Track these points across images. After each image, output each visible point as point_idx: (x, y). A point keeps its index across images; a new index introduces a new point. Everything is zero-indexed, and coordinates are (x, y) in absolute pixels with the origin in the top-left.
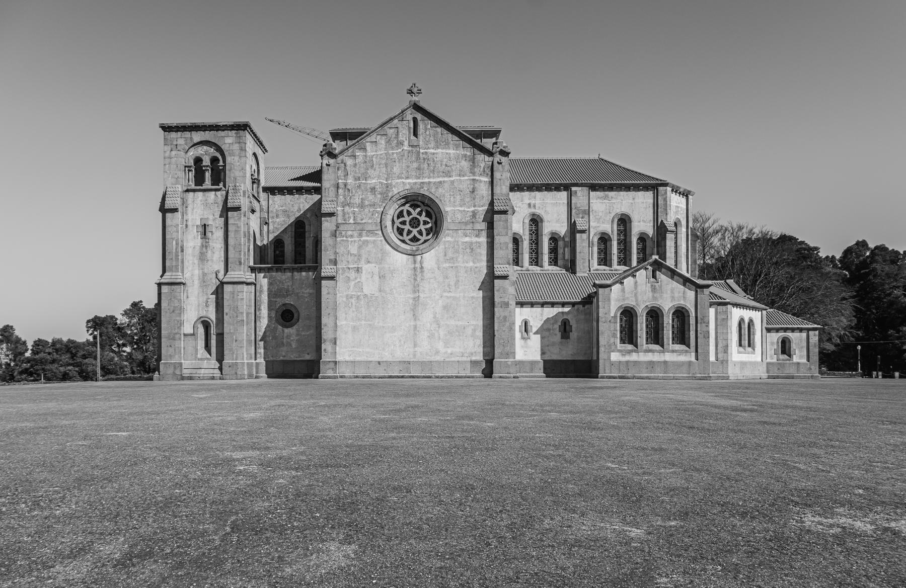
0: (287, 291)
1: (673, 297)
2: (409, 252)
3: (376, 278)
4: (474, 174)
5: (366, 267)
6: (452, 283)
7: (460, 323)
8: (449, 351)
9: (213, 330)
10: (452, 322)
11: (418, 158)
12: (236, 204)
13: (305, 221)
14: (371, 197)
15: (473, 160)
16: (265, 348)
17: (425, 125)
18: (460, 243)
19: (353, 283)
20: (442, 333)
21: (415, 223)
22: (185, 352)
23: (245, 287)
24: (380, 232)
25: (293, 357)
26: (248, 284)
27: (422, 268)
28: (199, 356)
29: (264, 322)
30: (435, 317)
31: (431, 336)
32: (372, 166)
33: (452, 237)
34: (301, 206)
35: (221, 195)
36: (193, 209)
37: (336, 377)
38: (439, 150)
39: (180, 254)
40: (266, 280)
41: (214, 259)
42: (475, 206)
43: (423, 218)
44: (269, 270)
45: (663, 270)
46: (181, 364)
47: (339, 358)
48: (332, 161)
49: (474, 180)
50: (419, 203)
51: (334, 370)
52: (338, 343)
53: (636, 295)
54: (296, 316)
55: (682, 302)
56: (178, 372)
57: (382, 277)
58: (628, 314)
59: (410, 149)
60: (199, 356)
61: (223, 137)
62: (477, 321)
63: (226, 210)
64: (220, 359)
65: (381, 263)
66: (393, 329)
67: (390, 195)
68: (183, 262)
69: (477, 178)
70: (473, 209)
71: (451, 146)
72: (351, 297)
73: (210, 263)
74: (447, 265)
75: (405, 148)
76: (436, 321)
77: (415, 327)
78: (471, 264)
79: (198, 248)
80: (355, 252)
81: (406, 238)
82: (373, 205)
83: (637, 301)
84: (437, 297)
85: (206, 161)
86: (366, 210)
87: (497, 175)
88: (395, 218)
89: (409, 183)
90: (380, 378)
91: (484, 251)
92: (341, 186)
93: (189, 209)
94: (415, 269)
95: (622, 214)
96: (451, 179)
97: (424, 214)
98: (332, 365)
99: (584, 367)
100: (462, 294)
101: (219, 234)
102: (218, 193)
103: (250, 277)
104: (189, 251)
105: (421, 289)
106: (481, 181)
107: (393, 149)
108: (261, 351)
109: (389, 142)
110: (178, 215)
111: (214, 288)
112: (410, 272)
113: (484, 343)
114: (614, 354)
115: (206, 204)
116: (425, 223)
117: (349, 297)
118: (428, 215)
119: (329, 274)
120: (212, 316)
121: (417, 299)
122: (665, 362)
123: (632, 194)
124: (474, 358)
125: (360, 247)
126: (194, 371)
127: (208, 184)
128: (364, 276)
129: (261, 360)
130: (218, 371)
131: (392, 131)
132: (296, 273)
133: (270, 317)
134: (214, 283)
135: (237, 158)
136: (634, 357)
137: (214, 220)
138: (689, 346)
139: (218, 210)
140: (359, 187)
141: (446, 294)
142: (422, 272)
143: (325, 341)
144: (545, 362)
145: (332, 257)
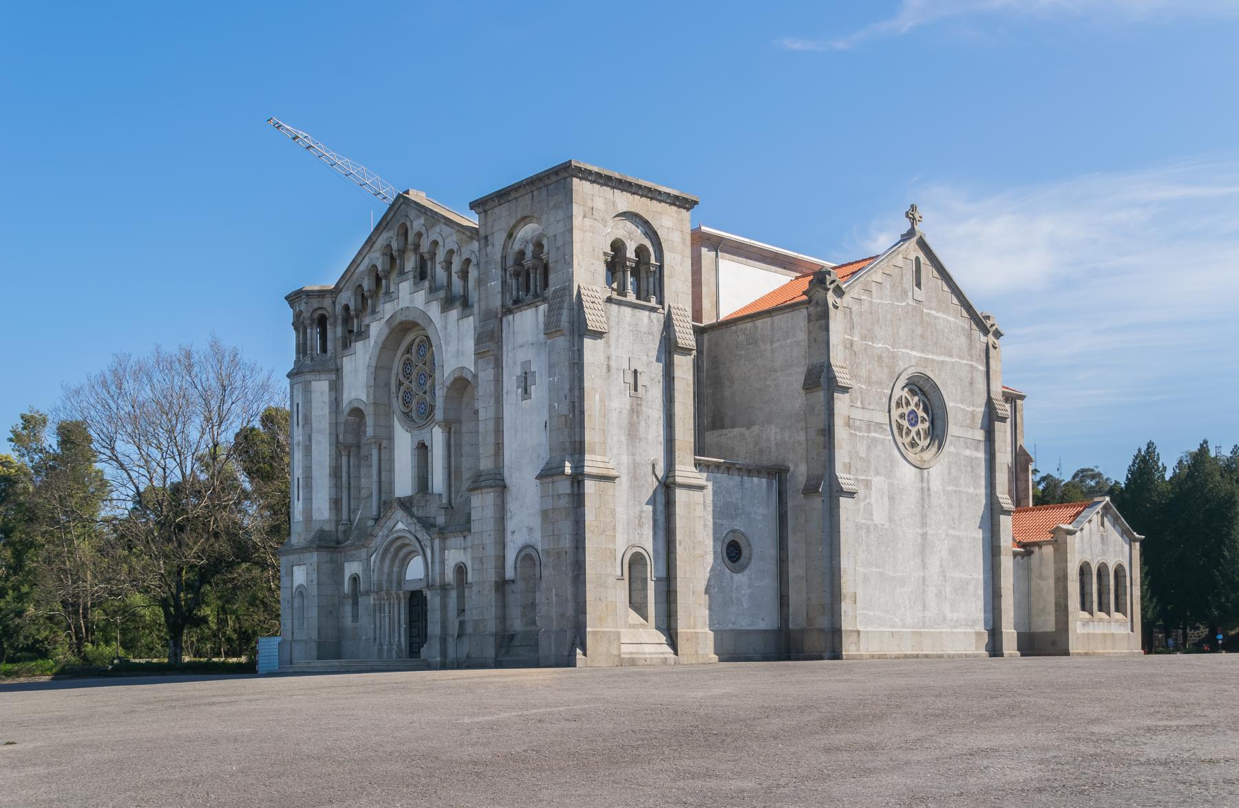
0: (737, 508)
2: (918, 464)
6: (956, 516)
7: (963, 576)
15: (970, 336)
17: (928, 271)
20: (948, 589)
25: (744, 624)
27: (929, 489)
36: (618, 338)
38: (940, 314)
43: (921, 413)
45: (775, 483)
49: (972, 366)
51: (858, 643)
54: (745, 553)
57: (892, 499)
58: (1084, 570)
62: (977, 575)
67: (897, 371)
70: (971, 409)
76: (943, 573)
77: (924, 578)
78: (971, 490)
80: (864, 455)
82: (880, 383)
91: (982, 472)
94: (922, 489)
98: (855, 635)
102: (654, 315)
106: (978, 370)
109: (893, 287)
111: (651, 493)
112: (918, 494)
113: (985, 605)
116: (923, 420)
118: (926, 410)
120: (647, 542)
121: (924, 536)
125: (869, 448)
127: (631, 297)
128: (874, 495)
131: (897, 270)
132: (745, 478)
134: (650, 485)
135: (678, 257)
136: (1091, 629)
137: (649, 364)
138: (1125, 614)
141: (950, 532)
142: (929, 495)
144: (1018, 634)
145: (847, 460)
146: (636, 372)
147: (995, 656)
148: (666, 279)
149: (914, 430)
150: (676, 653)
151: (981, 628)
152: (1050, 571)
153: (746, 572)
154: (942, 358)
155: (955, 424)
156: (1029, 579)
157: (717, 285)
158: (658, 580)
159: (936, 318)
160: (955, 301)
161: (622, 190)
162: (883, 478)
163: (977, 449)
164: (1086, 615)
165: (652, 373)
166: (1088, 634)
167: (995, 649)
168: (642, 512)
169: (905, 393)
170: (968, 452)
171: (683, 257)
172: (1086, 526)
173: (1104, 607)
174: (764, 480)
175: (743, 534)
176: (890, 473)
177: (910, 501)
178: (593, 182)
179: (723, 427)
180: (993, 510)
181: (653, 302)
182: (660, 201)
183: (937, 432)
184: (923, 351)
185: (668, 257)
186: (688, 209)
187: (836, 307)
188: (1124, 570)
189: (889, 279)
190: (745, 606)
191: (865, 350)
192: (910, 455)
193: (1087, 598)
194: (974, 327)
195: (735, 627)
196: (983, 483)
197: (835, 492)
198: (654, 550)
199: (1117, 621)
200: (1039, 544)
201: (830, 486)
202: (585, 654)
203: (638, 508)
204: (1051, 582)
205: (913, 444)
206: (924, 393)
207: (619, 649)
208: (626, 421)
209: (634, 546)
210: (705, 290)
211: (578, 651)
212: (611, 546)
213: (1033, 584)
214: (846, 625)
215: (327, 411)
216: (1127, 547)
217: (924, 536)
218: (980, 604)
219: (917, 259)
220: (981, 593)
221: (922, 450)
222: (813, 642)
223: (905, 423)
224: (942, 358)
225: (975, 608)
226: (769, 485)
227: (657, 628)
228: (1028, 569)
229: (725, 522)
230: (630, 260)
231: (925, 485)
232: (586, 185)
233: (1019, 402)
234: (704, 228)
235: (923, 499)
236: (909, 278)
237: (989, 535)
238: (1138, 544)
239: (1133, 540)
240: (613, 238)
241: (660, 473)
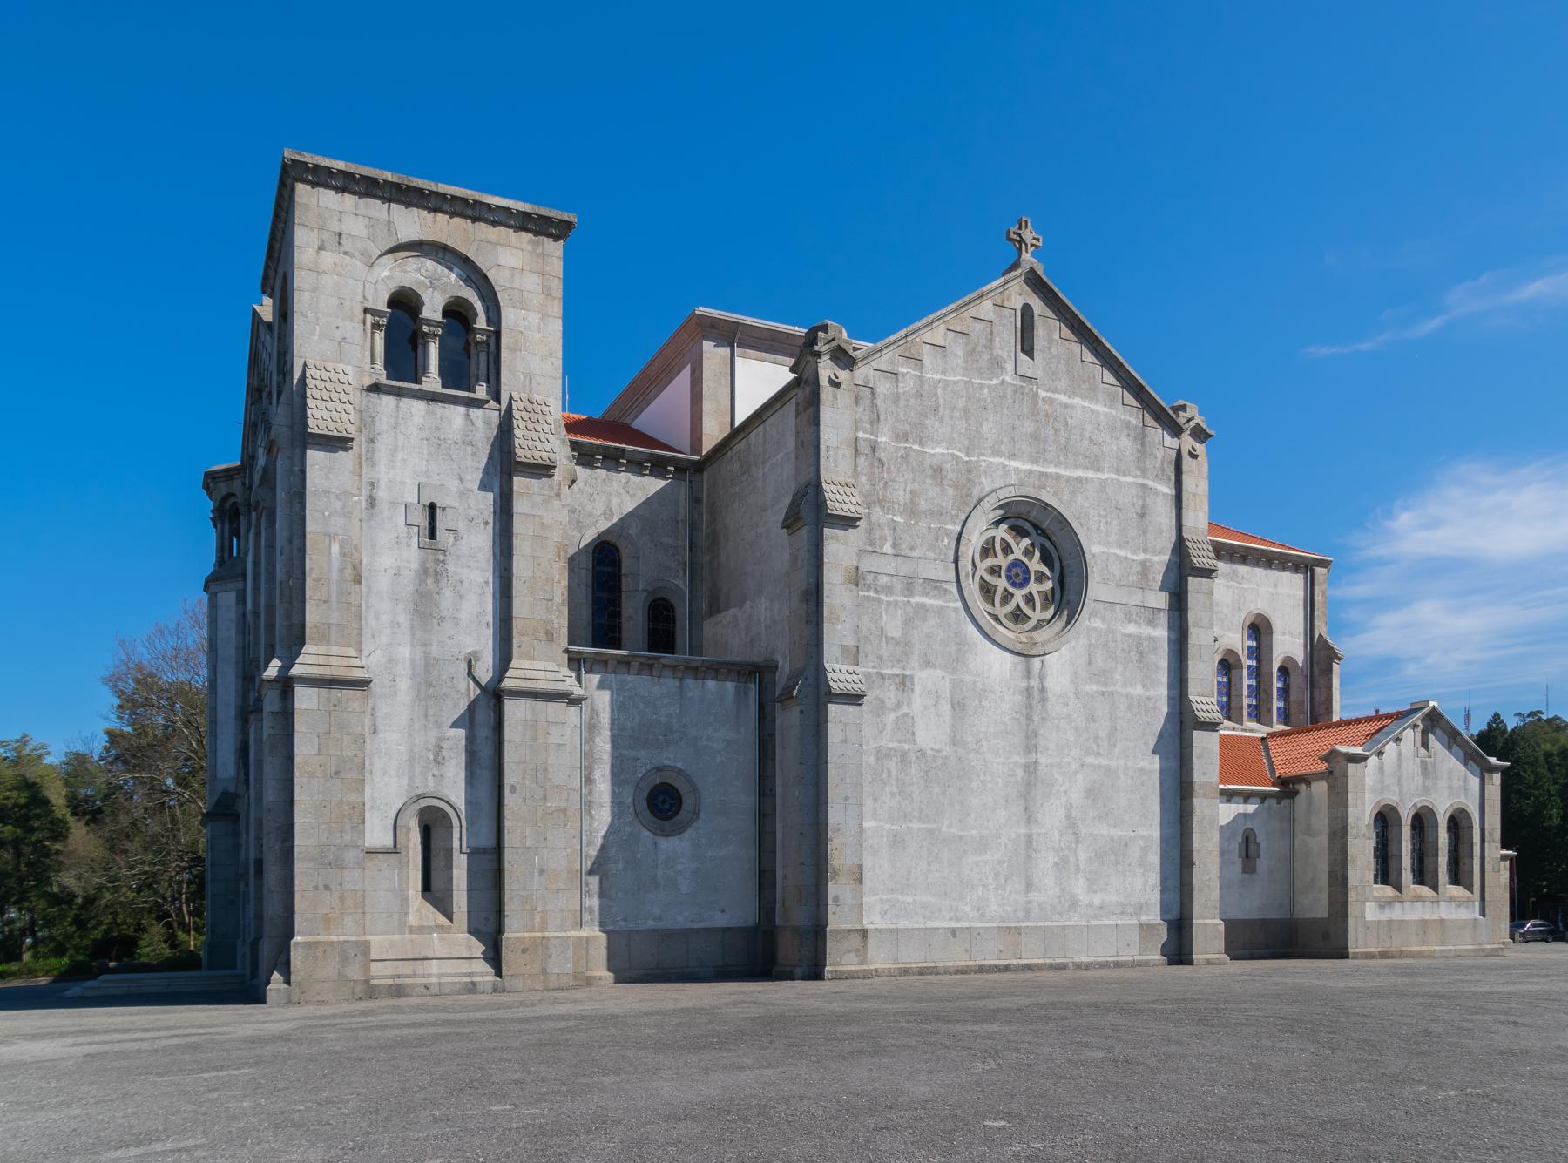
1: (1450, 787)
2: (1018, 647)
3: (946, 708)
4: (1144, 472)
5: (925, 678)
6: (1103, 734)
8: (1097, 900)
9: (459, 839)
10: (1103, 830)
11: (1034, 410)
12: (540, 457)
13: (621, 545)
14: (933, 492)
15: (1141, 438)
16: (603, 894)
17: (1049, 329)
18: (1118, 637)
19: (892, 716)
20: (1083, 856)
21: (1019, 575)
22: (361, 915)
24: (954, 589)
25: (682, 919)
27: (1043, 690)
28: (413, 920)
29: (603, 817)
30: (1068, 817)
31: (1061, 865)
32: (936, 410)
33: (1103, 619)
34: (615, 501)
35: (484, 422)
36: (394, 450)
37: (867, 975)
38: (1077, 401)
41: (463, 615)
42: (1145, 551)
43: (1035, 565)
44: (624, 663)
45: (753, 689)
46: (365, 947)
47: (866, 924)
48: (843, 375)
49: (1144, 486)
50: (1027, 526)
51: (862, 952)
52: (866, 880)
53: (1399, 781)
54: (688, 803)
55: (1462, 800)
56: (354, 972)
57: (958, 706)
58: (1385, 820)
59: (1017, 382)
60: (413, 920)
62: (1149, 829)
63: (505, 466)
64: (490, 931)
65: (955, 670)
66: (982, 845)
67: (976, 493)
69: (1150, 483)
70: (1141, 557)
71: (1100, 395)
72: (888, 756)
74: (1094, 688)
75: (1008, 379)
76: (1071, 825)
78: (1138, 690)
79: (409, 577)
80: (897, 634)
81: (1003, 611)
82: (938, 514)
83: (1401, 793)
84: (1074, 766)
85: (432, 310)
86: (923, 524)
87: (1187, 481)
88: (1032, 624)
89: (1017, 470)
90: (957, 972)
91: (1162, 660)
92: (864, 448)
93: (382, 448)
95: (1259, 615)
96: (1100, 475)
97: (1037, 554)
98: (855, 940)
99: (1292, 934)
100: (1122, 762)
101: (480, 541)
102: (477, 414)
103: (565, 680)
105: (1041, 742)
106: (1157, 493)
107: (981, 375)
109: (971, 353)
111: (462, 707)
112: (1019, 699)
113: (1164, 880)
114: (1373, 910)
115: (436, 441)
116: (1040, 577)
117: (882, 755)
118: (1046, 559)
120: (453, 788)
121: (1031, 768)
122: (1442, 921)
123: (1273, 574)
124: (1144, 918)
125: (908, 622)
126: (407, 968)
127: (432, 381)
128: (918, 701)
130: (483, 970)
131: (980, 326)
132: (689, 682)
133: (616, 802)
134: (462, 694)
135: (534, 318)
136: (1396, 913)
137: (463, 494)
138: (1470, 888)
139: (475, 463)
140: (905, 458)
141: (1090, 760)
142: (1044, 700)
143: (836, 874)
145: (850, 641)
146: (432, 508)
147: (1181, 962)
148: (504, 354)
149: (1019, 595)
150: (499, 973)
151: (1154, 916)
152: (1321, 822)
153: (686, 835)
154: (1078, 473)
155: (1105, 581)
156: (1291, 835)
157: (733, 398)
158: (473, 853)
159: (1066, 406)
160: (1110, 378)
161: (408, 205)
162: (939, 672)
163: (1151, 623)
164: (1389, 891)
165: (469, 513)
166: (1390, 922)
167: (1179, 950)
168: (443, 739)
169: (1002, 532)
170: (1131, 629)
171: (544, 316)
172: (1390, 748)
173: (1428, 878)
174: (730, 686)
175: (680, 772)
176: (957, 661)
177: (1003, 707)
178: (338, 190)
179: (718, 612)
180: (1182, 722)
181: (481, 391)
182: (494, 224)
183: (1067, 593)
184: (1036, 462)
185: (509, 316)
186: (557, 238)
187: (835, 384)
188: (1469, 817)
189: (961, 340)
190: (684, 889)
191: (905, 458)
192: (1006, 633)
193: (1392, 864)
194: (1150, 421)
195: (661, 925)
196: (1164, 678)
197: (821, 695)
198: (468, 802)
199: (1451, 899)
200: (1305, 780)
201: (818, 686)
202: (288, 982)
203: (433, 735)
204: (1323, 840)
205: (1018, 617)
206: (1044, 533)
207: (367, 969)
208: (410, 589)
209: (420, 797)
210: (707, 406)
211: (276, 976)
212: (353, 797)
213: (1297, 842)
214: (837, 920)
215: (233, 632)
216: (1475, 782)
217: (1031, 768)
218: (1154, 878)
219: (1027, 310)
220: (1155, 859)
221: (1036, 628)
222: (788, 949)
223: (1002, 583)
224: (1078, 473)
225: (1142, 888)
226: (741, 695)
227: (473, 931)
228: (1290, 819)
229: (642, 754)
230: (429, 322)
231: (1035, 683)
232: (328, 199)
233: (1319, 571)
234: (702, 310)
235: (1030, 707)
236: (1007, 338)
237: (1174, 764)
238: (1497, 777)
239: (1488, 769)
240: (392, 287)
241: (485, 672)
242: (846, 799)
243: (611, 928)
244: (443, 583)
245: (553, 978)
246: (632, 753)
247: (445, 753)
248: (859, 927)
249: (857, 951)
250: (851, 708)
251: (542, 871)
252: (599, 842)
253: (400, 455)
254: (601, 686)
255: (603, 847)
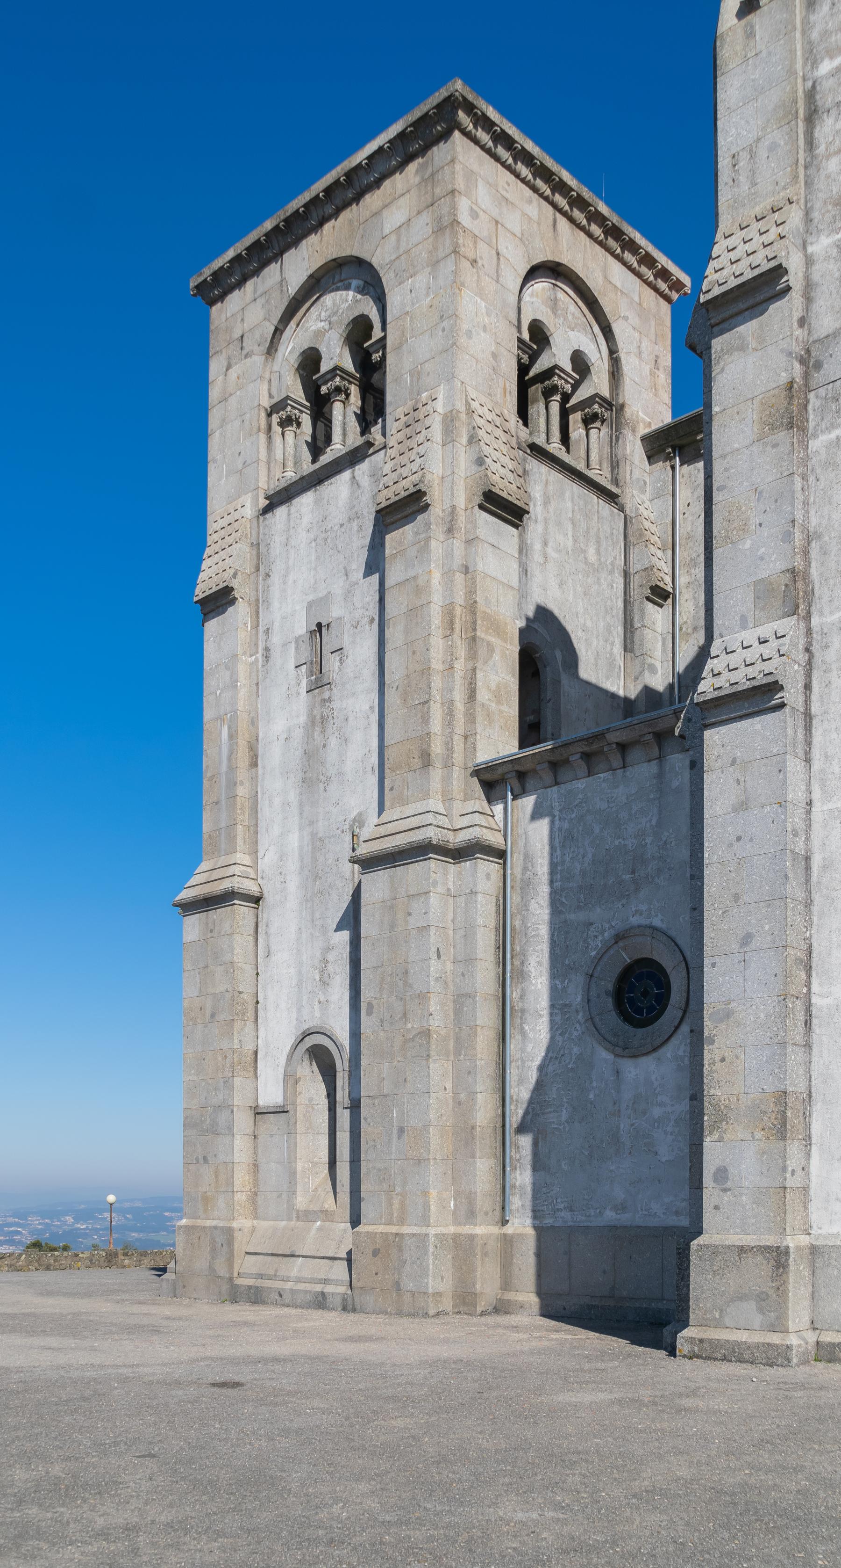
16: (538, 1164)
23: (434, 866)
26: (459, 854)
28: (301, 1201)
29: (534, 1038)
39: (242, 774)
40: (544, 825)
46: (229, 1232)
60: (301, 1201)
61: (377, 214)
68: (255, 810)
73: (333, 787)
98: (757, 1272)
101: (363, 650)
103: (469, 815)
104: (274, 756)
108: (523, 1178)
110: (239, 612)
119: (742, 679)
120: (341, 1030)
129: (521, 1225)
195: (625, 1219)
214: (727, 1223)
242: (746, 940)
243: (549, 1221)
244: (329, 731)
245: (407, 1298)
246: (582, 916)
247: (330, 967)
248: (770, 1240)
249: (762, 1298)
250: (756, 724)
251: (401, 1130)
252: (533, 1076)
253: (291, 578)
254: (536, 815)
255: (539, 1086)
